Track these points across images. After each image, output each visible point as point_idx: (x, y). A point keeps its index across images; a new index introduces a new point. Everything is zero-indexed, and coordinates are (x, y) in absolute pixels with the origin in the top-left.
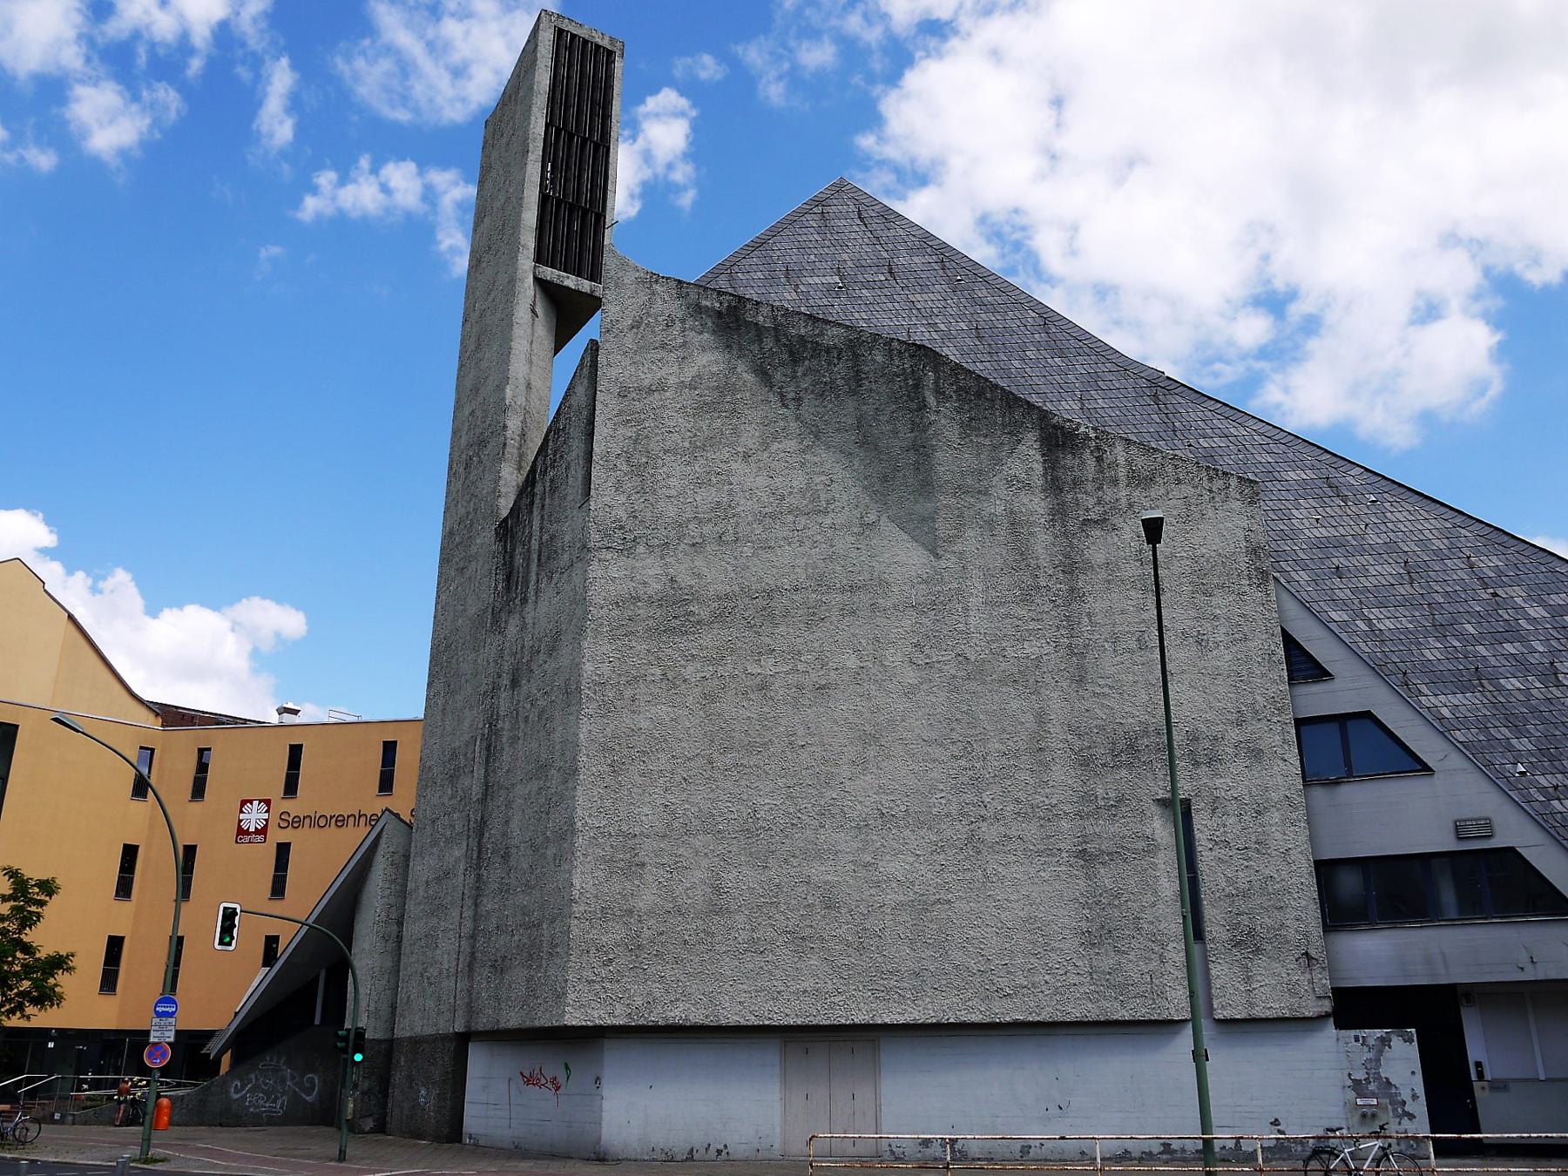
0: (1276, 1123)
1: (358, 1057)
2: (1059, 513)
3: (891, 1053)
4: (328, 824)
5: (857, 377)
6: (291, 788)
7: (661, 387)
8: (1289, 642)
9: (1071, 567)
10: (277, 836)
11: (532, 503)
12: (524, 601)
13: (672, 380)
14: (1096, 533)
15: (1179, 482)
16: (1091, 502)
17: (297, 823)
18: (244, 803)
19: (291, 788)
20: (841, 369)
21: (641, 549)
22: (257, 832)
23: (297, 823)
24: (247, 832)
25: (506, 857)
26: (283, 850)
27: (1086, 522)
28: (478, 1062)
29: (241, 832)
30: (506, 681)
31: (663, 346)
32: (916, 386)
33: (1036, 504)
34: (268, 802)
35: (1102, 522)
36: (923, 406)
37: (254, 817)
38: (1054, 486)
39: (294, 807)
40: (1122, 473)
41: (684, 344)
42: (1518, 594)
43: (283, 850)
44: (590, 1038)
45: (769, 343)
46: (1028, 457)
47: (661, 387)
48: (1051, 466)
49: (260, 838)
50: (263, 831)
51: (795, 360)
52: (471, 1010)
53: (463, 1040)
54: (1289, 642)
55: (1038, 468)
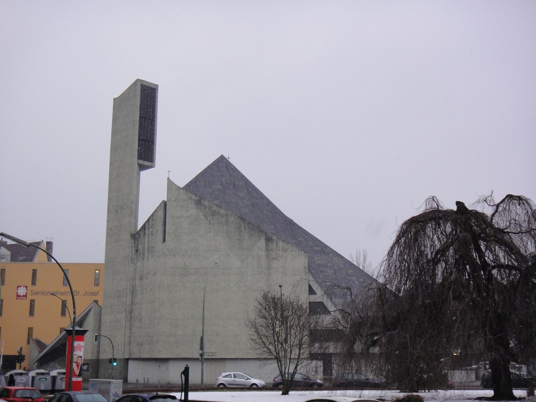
0: (280, 286)
1: (115, 364)
2: (268, 256)
3: (228, 364)
4: (47, 294)
5: (227, 222)
6: (34, 283)
7: (182, 217)
8: (310, 287)
9: (269, 268)
10: (30, 297)
11: (145, 235)
12: (143, 259)
13: (184, 216)
14: (275, 261)
15: (292, 251)
16: (274, 254)
17: (37, 293)
18: (18, 287)
19: (34, 283)
20: (224, 219)
21: (177, 256)
22: (23, 296)
23: (37, 293)
24: (20, 296)
25: (141, 320)
26: (32, 302)
27: (273, 258)
28: (131, 363)
29: (18, 296)
30: (138, 277)
31: (182, 206)
32: (240, 226)
33: (263, 253)
34: (26, 287)
35: (276, 259)
36: (241, 231)
37: (22, 291)
38: (267, 250)
39: (35, 288)
40: (281, 248)
41: (187, 207)
42: (354, 278)
43: (32, 302)
44: (166, 360)
45: (207, 210)
46: (262, 243)
47: (182, 217)
48: (267, 245)
49: (24, 298)
50: (25, 296)
51: (213, 215)
52: (130, 353)
53: (127, 360)
54: (310, 287)
55: (264, 245)
